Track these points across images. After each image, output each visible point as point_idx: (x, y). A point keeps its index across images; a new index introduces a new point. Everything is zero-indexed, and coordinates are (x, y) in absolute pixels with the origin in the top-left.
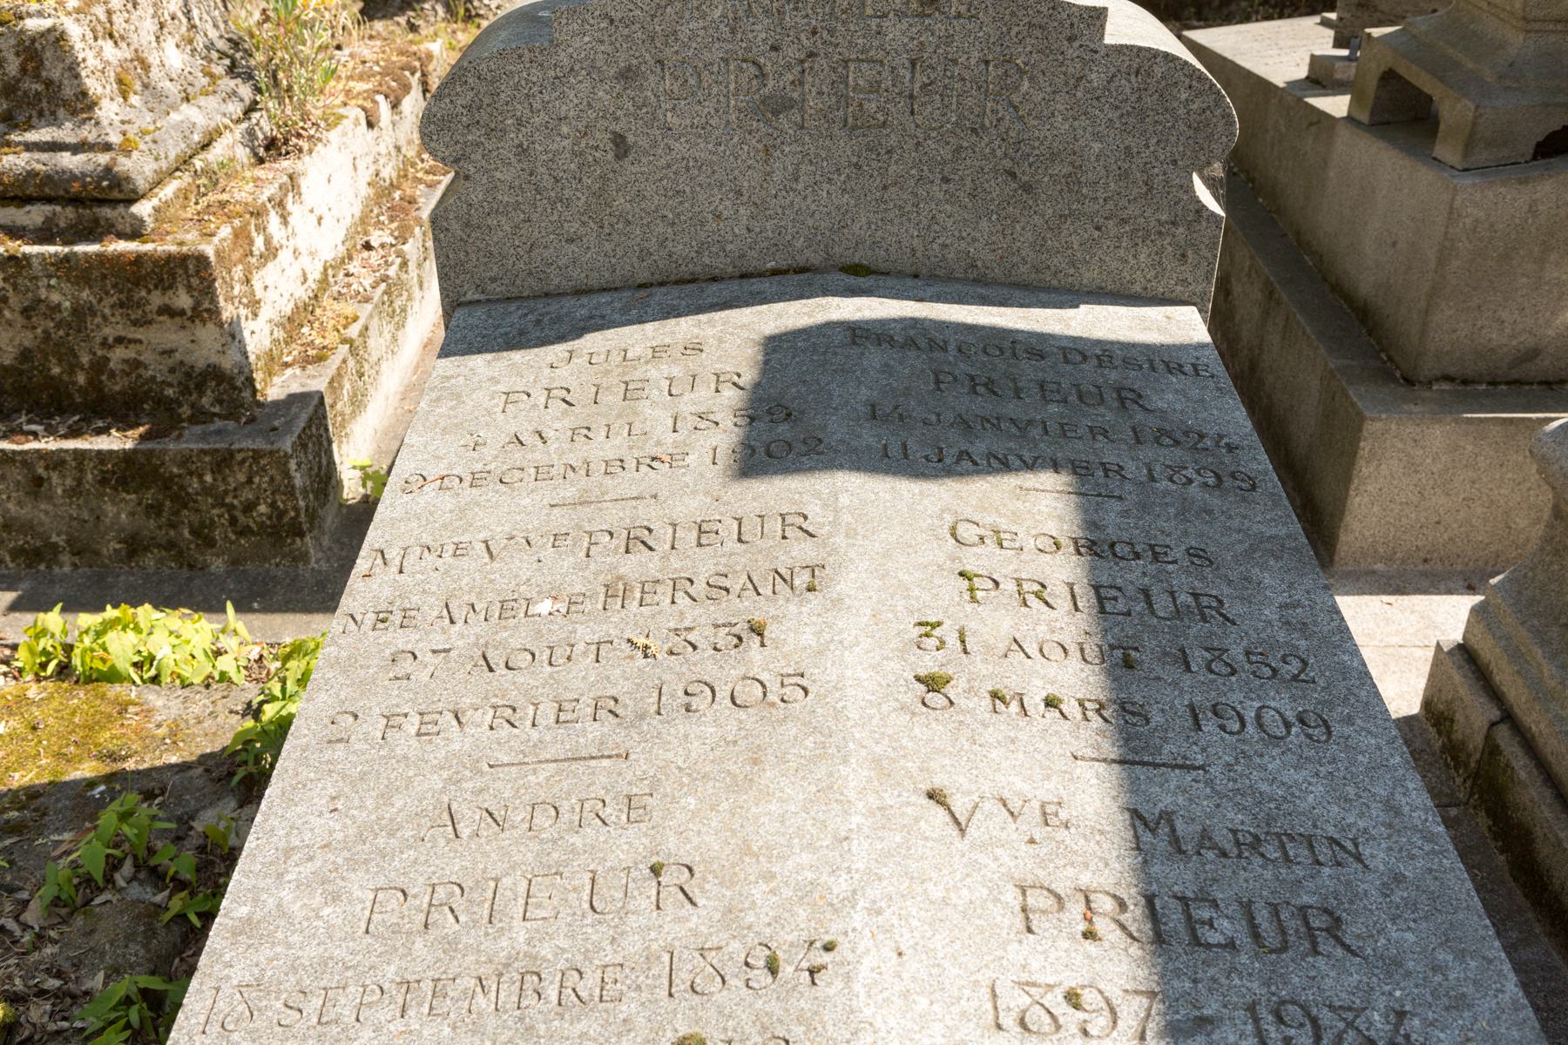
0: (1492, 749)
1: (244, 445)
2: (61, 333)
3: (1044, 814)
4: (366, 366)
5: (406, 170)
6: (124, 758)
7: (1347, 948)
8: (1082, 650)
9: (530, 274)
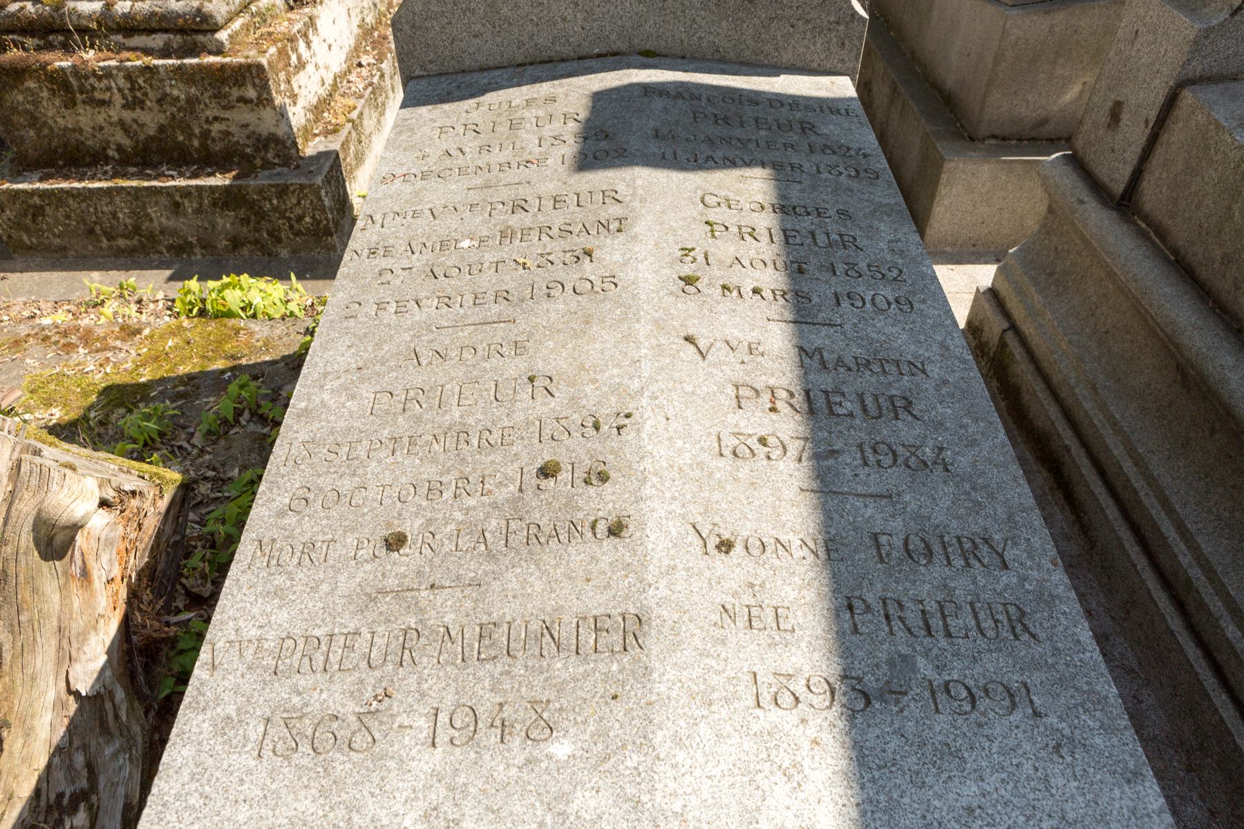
0: (1003, 344)
1: (294, 181)
2: (181, 115)
3: (750, 349)
4: (363, 137)
5: (380, 19)
6: (240, 358)
7: (915, 417)
8: (775, 264)
9: (453, 58)
